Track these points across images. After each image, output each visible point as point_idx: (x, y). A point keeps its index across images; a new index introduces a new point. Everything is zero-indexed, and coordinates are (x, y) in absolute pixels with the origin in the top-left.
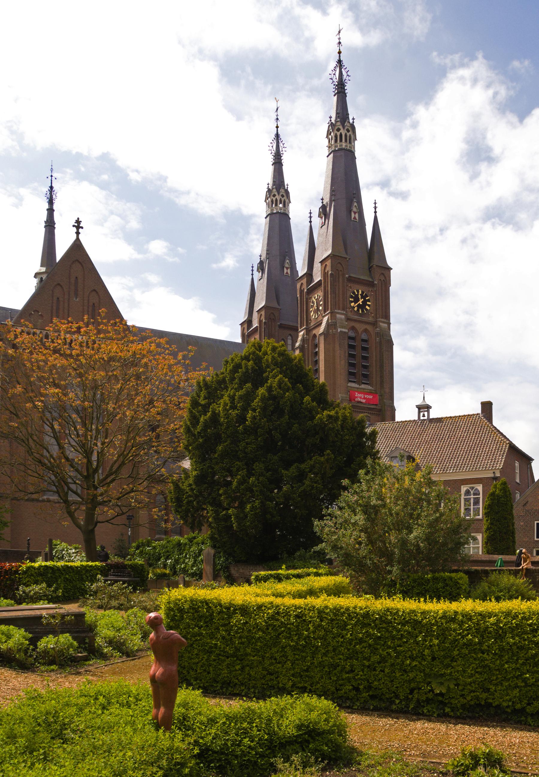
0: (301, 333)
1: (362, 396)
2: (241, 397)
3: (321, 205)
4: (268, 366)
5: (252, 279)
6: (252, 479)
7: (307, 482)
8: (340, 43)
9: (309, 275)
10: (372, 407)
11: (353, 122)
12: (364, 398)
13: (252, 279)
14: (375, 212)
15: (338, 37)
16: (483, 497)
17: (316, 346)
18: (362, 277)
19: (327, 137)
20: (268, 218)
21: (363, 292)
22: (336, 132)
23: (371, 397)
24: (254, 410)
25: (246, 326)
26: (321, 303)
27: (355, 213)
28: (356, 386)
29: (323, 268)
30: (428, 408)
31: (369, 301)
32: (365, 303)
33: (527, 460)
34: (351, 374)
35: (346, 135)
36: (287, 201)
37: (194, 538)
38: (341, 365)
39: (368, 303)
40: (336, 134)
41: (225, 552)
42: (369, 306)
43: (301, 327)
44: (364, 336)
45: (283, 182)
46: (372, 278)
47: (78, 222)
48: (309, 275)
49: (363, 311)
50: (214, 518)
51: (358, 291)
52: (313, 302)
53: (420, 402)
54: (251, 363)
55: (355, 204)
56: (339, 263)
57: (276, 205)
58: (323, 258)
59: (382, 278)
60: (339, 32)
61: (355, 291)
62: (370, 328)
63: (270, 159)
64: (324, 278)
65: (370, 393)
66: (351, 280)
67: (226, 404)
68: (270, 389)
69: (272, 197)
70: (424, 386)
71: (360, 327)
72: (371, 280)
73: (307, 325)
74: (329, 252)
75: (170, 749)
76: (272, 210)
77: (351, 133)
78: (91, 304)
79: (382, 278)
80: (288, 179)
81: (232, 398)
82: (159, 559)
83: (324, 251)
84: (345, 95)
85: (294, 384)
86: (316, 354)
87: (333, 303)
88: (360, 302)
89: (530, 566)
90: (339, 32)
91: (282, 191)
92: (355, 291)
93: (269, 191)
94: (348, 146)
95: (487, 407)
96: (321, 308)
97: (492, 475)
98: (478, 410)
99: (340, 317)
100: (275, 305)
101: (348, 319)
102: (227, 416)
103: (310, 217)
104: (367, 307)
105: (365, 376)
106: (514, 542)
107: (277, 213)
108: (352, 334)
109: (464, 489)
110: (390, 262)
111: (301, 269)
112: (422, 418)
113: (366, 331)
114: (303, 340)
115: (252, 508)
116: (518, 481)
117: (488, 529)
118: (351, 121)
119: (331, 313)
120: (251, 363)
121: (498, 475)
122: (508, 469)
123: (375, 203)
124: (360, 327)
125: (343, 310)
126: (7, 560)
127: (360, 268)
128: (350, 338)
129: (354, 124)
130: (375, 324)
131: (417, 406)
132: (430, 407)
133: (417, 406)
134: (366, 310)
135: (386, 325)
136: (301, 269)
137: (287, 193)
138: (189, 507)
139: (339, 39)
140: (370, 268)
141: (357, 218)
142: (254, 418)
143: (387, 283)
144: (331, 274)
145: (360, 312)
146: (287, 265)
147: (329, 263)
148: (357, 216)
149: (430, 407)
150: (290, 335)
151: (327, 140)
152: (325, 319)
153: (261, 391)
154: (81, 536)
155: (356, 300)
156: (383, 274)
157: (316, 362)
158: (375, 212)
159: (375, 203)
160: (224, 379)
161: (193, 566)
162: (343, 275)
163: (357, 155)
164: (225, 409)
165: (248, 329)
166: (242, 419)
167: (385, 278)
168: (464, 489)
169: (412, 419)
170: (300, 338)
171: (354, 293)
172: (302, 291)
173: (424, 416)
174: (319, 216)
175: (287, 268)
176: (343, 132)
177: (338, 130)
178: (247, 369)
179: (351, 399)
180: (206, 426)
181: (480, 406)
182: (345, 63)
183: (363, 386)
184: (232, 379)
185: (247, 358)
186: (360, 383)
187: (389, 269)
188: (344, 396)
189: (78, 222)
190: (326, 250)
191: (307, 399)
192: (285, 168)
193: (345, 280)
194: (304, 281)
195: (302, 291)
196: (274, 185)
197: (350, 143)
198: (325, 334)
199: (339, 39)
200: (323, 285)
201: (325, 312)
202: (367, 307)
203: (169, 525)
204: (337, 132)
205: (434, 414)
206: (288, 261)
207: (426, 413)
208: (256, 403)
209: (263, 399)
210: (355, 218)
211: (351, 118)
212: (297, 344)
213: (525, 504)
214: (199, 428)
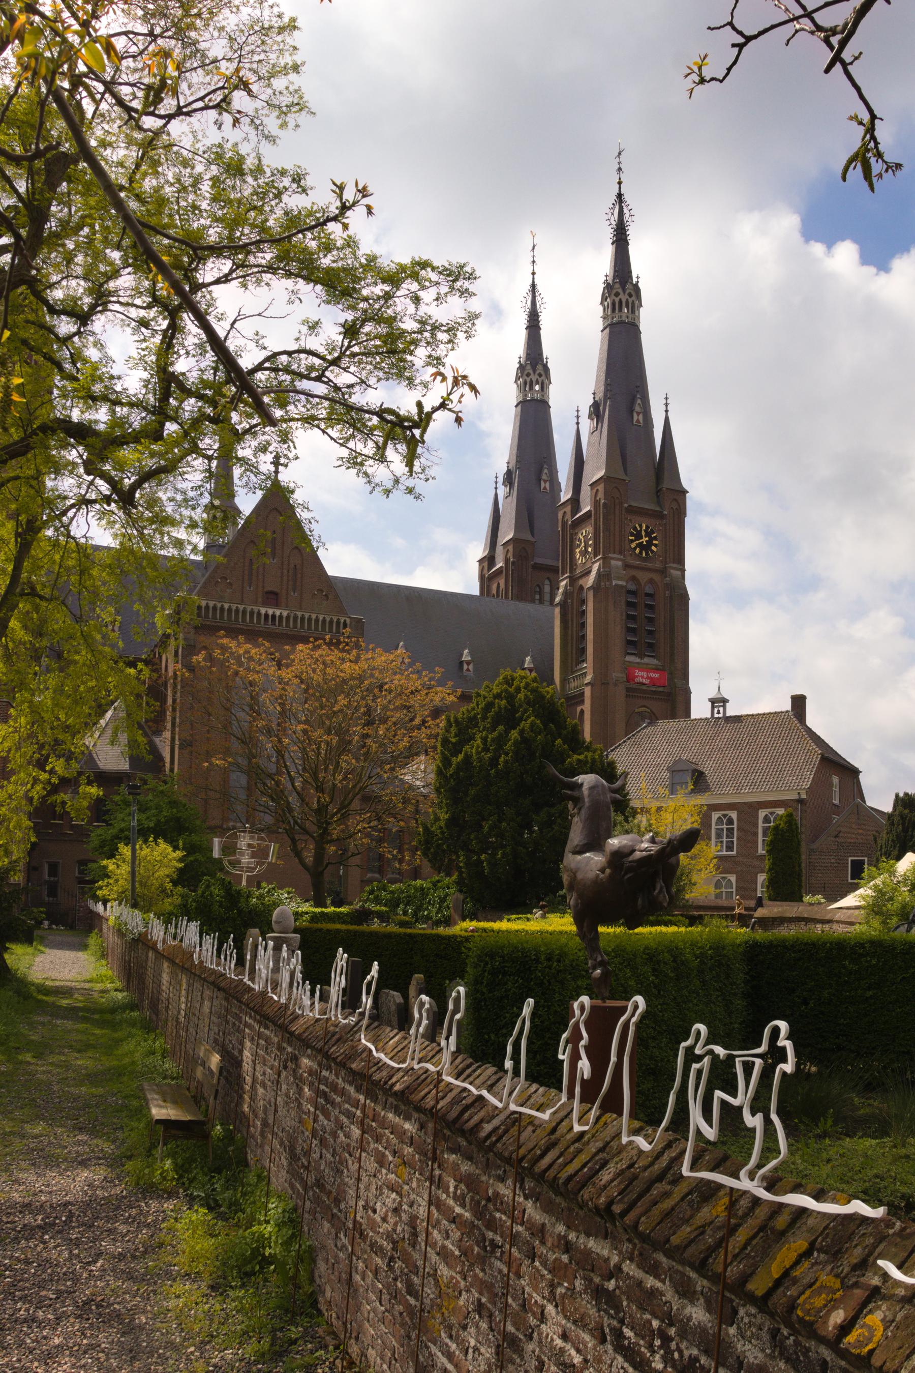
0: (563, 583)
1: (645, 674)
2: (493, 740)
3: (591, 401)
4: (521, 706)
5: (496, 495)
6: (504, 824)
7: (556, 828)
8: (620, 169)
9: (575, 502)
10: (658, 689)
12: (648, 678)
13: (496, 495)
16: (757, 824)
17: (583, 602)
18: (646, 506)
19: (602, 303)
21: (647, 527)
23: (657, 676)
24: (507, 754)
25: (486, 564)
27: (638, 414)
28: (637, 660)
30: (724, 701)
31: (655, 538)
32: (650, 543)
33: (851, 773)
34: (629, 643)
35: (627, 302)
36: (546, 381)
37: (439, 881)
38: (617, 632)
41: (472, 898)
42: (656, 545)
43: (563, 574)
44: (648, 589)
45: (541, 354)
46: (661, 507)
47: (460, 424)
48: (575, 502)
49: (647, 554)
50: (465, 863)
51: (641, 526)
52: (580, 540)
53: (713, 694)
54: (504, 702)
55: (639, 401)
57: (531, 388)
58: (594, 479)
62: (656, 577)
63: (608, 234)
65: (656, 670)
66: (632, 510)
67: (478, 747)
68: (522, 732)
70: (734, 658)
71: (644, 577)
72: (658, 509)
74: (601, 473)
76: (525, 396)
77: (634, 298)
78: (292, 566)
79: (675, 506)
81: (484, 740)
82: (398, 906)
83: (595, 472)
84: (626, 243)
85: (545, 726)
86: (583, 613)
87: (607, 544)
88: (645, 540)
89: (743, 912)
91: (540, 368)
93: (521, 368)
95: (799, 702)
97: (797, 797)
98: (787, 706)
99: (616, 563)
100: (529, 537)
101: (627, 566)
102: (480, 760)
103: (578, 417)
104: (653, 548)
105: (650, 646)
106: (800, 886)
107: (533, 400)
108: (632, 587)
109: (762, 813)
110: (685, 484)
111: (565, 495)
112: (716, 715)
113: (651, 581)
114: (566, 593)
115: (504, 854)
116: (836, 802)
117: (770, 870)
118: (635, 280)
119: (604, 558)
120: (504, 702)
121: (804, 796)
122: (820, 785)
123: (666, 398)
124: (644, 577)
125: (620, 553)
127: (645, 495)
128: (629, 592)
130: (663, 572)
131: (710, 700)
132: (727, 701)
133: (710, 700)
134: (652, 551)
135: (679, 573)
136: (565, 495)
138: (438, 852)
139: (620, 163)
140: (658, 492)
142: (506, 762)
143: (680, 513)
144: (604, 504)
147: (601, 487)
148: (641, 417)
149: (727, 701)
151: (601, 308)
152: (596, 567)
153: (514, 734)
154: (306, 878)
155: (638, 536)
156: (675, 500)
157: (583, 625)
158: (667, 411)
159: (666, 398)
160: (475, 717)
161: (437, 913)
162: (621, 504)
163: (641, 329)
164: (478, 753)
165: (489, 569)
166: (494, 761)
168: (762, 813)
169: (704, 717)
170: (561, 590)
171: (635, 529)
172: (564, 523)
173: (719, 712)
174: (590, 417)
175: (545, 481)
176: (624, 298)
177: (617, 294)
178: (500, 707)
179: (630, 678)
180: (459, 768)
181: (790, 700)
183: (646, 660)
184: (484, 718)
185: (498, 696)
186: (641, 656)
187: (684, 492)
188: (620, 675)
189: (460, 424)
190: (598, 469)
191: (559, 741)
194: (568, 509)
195: (564, 523)
196: (527, 359)
197: (633, 312)
198: (596, 588)
199: (620, 163)
201: (595, 556)
202: (653, 548)
203: (405, 866)
205: (732, 710)
206: (546, 471)
207: (721, 709)
208: (509, 746)
209: (516, 743)
210: (638, 421)
212: (558, 599)
213: (837, 835)
214: (452, 770)
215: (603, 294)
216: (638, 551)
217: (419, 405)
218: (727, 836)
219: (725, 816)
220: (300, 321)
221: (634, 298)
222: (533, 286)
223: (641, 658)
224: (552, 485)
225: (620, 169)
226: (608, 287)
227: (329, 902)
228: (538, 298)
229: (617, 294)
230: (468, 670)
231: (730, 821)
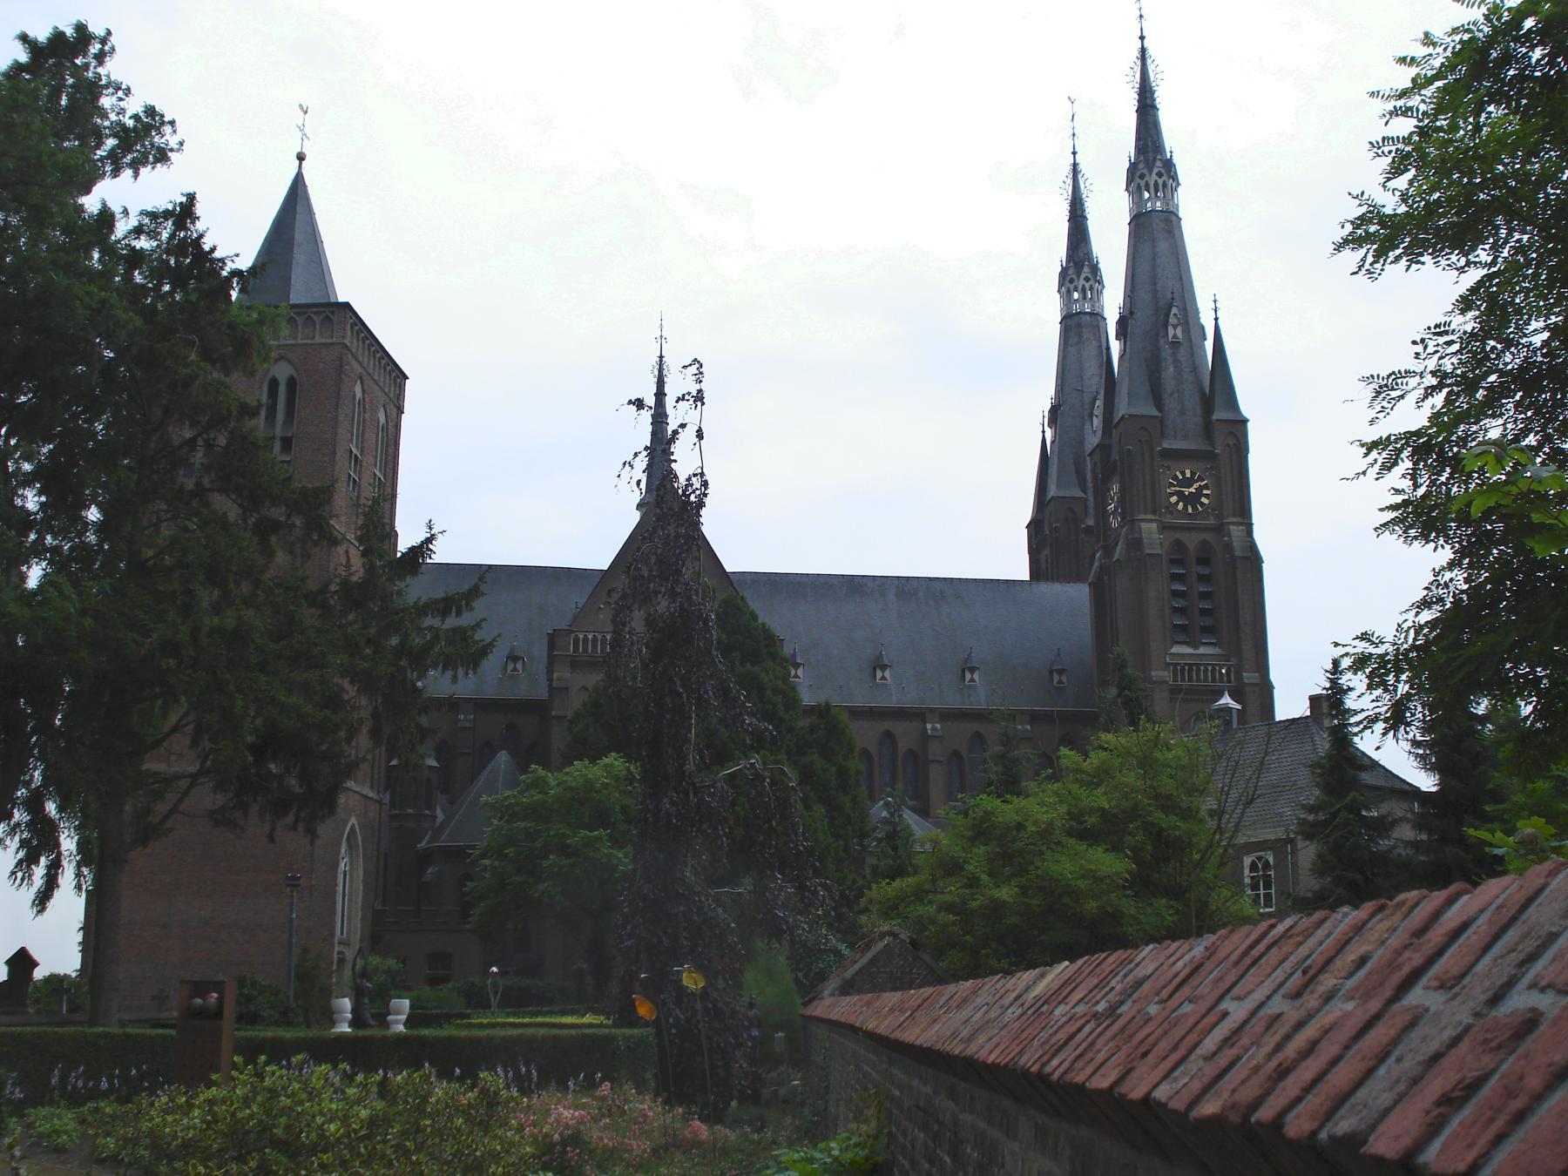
27: (1175, 327)
42: (1207, 496)
59: (1232, 442)
69: (1137, 180)
75: (347, 1135)
93: (1063, 274)
101: (1164, 528)
104: (1204, 500)
125: (1154, 513)
126: (1122, 490)
130: (1220, 529)
134: (1202, 504)
146: (1172, 320)
148: (1179, 331)
168: (1247, 861)
202: (1204, 500)
210: (1175, 336)
217: (455, 679)
219: (1259, 858)
220: (31, 913)
222: (1143, 50)
223: (1196, 648)
224: (1187, 331)
226: (1133, 172)
228: (1151, 68)
230: (972, 680)
231: (1267, 866)
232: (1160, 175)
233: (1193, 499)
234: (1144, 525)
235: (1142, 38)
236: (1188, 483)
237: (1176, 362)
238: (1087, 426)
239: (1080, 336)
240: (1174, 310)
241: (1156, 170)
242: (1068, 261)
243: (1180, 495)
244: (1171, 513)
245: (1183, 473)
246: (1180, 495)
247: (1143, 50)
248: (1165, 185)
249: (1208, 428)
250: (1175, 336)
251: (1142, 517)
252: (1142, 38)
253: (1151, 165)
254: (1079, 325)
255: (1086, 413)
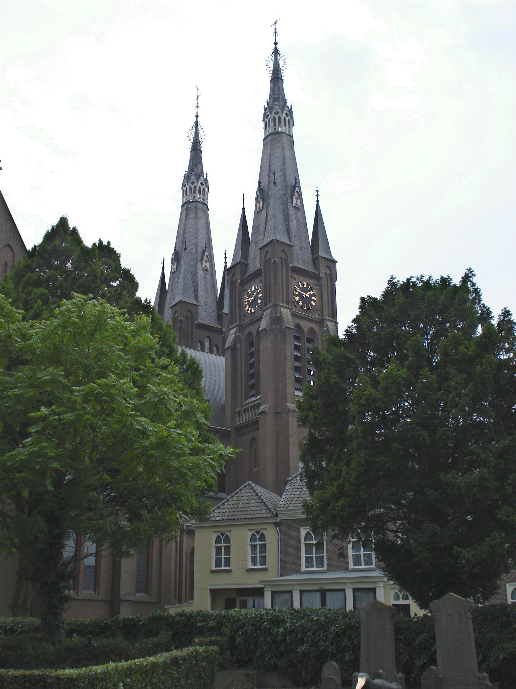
11: (291, 108)
14: (318, 201)
15: (274, 27)
16: (299, 542)
20: (185, 206)
22: (190, 184)
26: (260, 295)
27: (206, 262)
29: (263, 256)
39: (313, 298)
40: (274, 117)
42: (314, 301)
46: (317, 270)
49: (308, 306)
56: (283, 250)
60: (198, 98)
61: (300, 283)
62: (316, 327)
63: (267, 76)
64: (265, 267)
66: (297, 271)
73: (240, 321)
77: (204, 186)
80: (208, 166)
90: (198, 98)
92: (300, 283)
94: (287, 130)
96: (259, 301)
101: (294, 315)
118: (205, 176)
123: (317, 191)
129: (208, 178)
130: (321, 323)
134: (312, 305)
137: (206, 181)
141: (299, 205)
143: (332, 278)
145: (306, 308)
146: (205, 258)
148: (208, 264)
150: (208, 337)
151: (181, 191)
159: (317, 191)
162: (287, 264)
167: (331, 271)
182: (281, 51)
187: (335, 262)
192: (204, 157)
193: (290, 271)
200: (263, 274)
204: (191, 185)
210: (296, 204)
211: (288, 104)
215: (183, 183)
216: (301, 303)
218: (261, 553)
221: (204, 186)
222: (197, 123)
225: (275, 33)
226: (187, 177)
227: (173, 647)
228: (200, 132)
229: (193, 183)
232: (202, 184)
233: (309, 299)
234: (283, 310)
235: (197, 116)
236: (306, 290)
237: (296, 218)
238: (199, 265)
239: (196, 214)
240: (206, 253)
241: (200, 181)
242: (270, 99)
243: (300, 295)
244: (295, 306)
245: (302, 284)
246: (300, 295)
247: (197, 123)
248: (204, 190)
249: (315, 260)
250: (296, 204)
251: (281, 304)
252: (197, 116)
253: (278, 114)
254: (196, 208)
255: (199, 258)
